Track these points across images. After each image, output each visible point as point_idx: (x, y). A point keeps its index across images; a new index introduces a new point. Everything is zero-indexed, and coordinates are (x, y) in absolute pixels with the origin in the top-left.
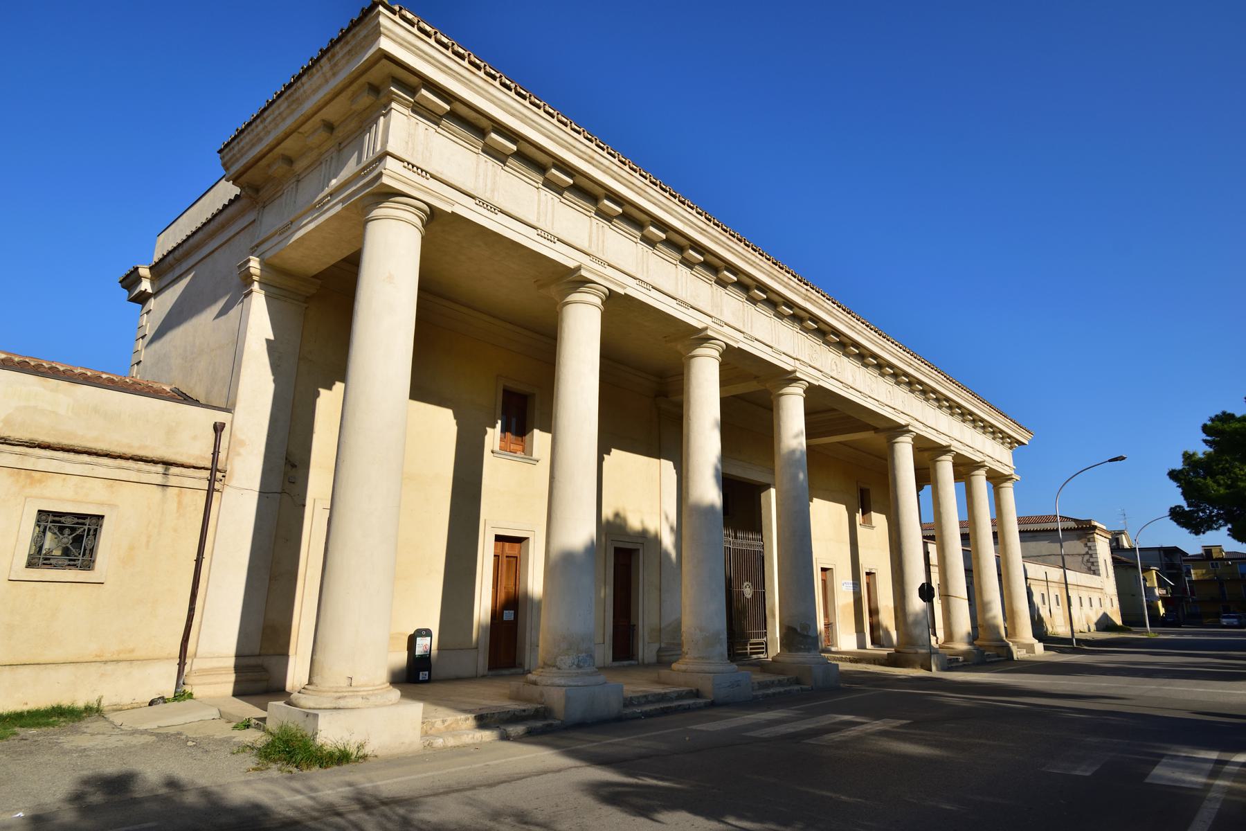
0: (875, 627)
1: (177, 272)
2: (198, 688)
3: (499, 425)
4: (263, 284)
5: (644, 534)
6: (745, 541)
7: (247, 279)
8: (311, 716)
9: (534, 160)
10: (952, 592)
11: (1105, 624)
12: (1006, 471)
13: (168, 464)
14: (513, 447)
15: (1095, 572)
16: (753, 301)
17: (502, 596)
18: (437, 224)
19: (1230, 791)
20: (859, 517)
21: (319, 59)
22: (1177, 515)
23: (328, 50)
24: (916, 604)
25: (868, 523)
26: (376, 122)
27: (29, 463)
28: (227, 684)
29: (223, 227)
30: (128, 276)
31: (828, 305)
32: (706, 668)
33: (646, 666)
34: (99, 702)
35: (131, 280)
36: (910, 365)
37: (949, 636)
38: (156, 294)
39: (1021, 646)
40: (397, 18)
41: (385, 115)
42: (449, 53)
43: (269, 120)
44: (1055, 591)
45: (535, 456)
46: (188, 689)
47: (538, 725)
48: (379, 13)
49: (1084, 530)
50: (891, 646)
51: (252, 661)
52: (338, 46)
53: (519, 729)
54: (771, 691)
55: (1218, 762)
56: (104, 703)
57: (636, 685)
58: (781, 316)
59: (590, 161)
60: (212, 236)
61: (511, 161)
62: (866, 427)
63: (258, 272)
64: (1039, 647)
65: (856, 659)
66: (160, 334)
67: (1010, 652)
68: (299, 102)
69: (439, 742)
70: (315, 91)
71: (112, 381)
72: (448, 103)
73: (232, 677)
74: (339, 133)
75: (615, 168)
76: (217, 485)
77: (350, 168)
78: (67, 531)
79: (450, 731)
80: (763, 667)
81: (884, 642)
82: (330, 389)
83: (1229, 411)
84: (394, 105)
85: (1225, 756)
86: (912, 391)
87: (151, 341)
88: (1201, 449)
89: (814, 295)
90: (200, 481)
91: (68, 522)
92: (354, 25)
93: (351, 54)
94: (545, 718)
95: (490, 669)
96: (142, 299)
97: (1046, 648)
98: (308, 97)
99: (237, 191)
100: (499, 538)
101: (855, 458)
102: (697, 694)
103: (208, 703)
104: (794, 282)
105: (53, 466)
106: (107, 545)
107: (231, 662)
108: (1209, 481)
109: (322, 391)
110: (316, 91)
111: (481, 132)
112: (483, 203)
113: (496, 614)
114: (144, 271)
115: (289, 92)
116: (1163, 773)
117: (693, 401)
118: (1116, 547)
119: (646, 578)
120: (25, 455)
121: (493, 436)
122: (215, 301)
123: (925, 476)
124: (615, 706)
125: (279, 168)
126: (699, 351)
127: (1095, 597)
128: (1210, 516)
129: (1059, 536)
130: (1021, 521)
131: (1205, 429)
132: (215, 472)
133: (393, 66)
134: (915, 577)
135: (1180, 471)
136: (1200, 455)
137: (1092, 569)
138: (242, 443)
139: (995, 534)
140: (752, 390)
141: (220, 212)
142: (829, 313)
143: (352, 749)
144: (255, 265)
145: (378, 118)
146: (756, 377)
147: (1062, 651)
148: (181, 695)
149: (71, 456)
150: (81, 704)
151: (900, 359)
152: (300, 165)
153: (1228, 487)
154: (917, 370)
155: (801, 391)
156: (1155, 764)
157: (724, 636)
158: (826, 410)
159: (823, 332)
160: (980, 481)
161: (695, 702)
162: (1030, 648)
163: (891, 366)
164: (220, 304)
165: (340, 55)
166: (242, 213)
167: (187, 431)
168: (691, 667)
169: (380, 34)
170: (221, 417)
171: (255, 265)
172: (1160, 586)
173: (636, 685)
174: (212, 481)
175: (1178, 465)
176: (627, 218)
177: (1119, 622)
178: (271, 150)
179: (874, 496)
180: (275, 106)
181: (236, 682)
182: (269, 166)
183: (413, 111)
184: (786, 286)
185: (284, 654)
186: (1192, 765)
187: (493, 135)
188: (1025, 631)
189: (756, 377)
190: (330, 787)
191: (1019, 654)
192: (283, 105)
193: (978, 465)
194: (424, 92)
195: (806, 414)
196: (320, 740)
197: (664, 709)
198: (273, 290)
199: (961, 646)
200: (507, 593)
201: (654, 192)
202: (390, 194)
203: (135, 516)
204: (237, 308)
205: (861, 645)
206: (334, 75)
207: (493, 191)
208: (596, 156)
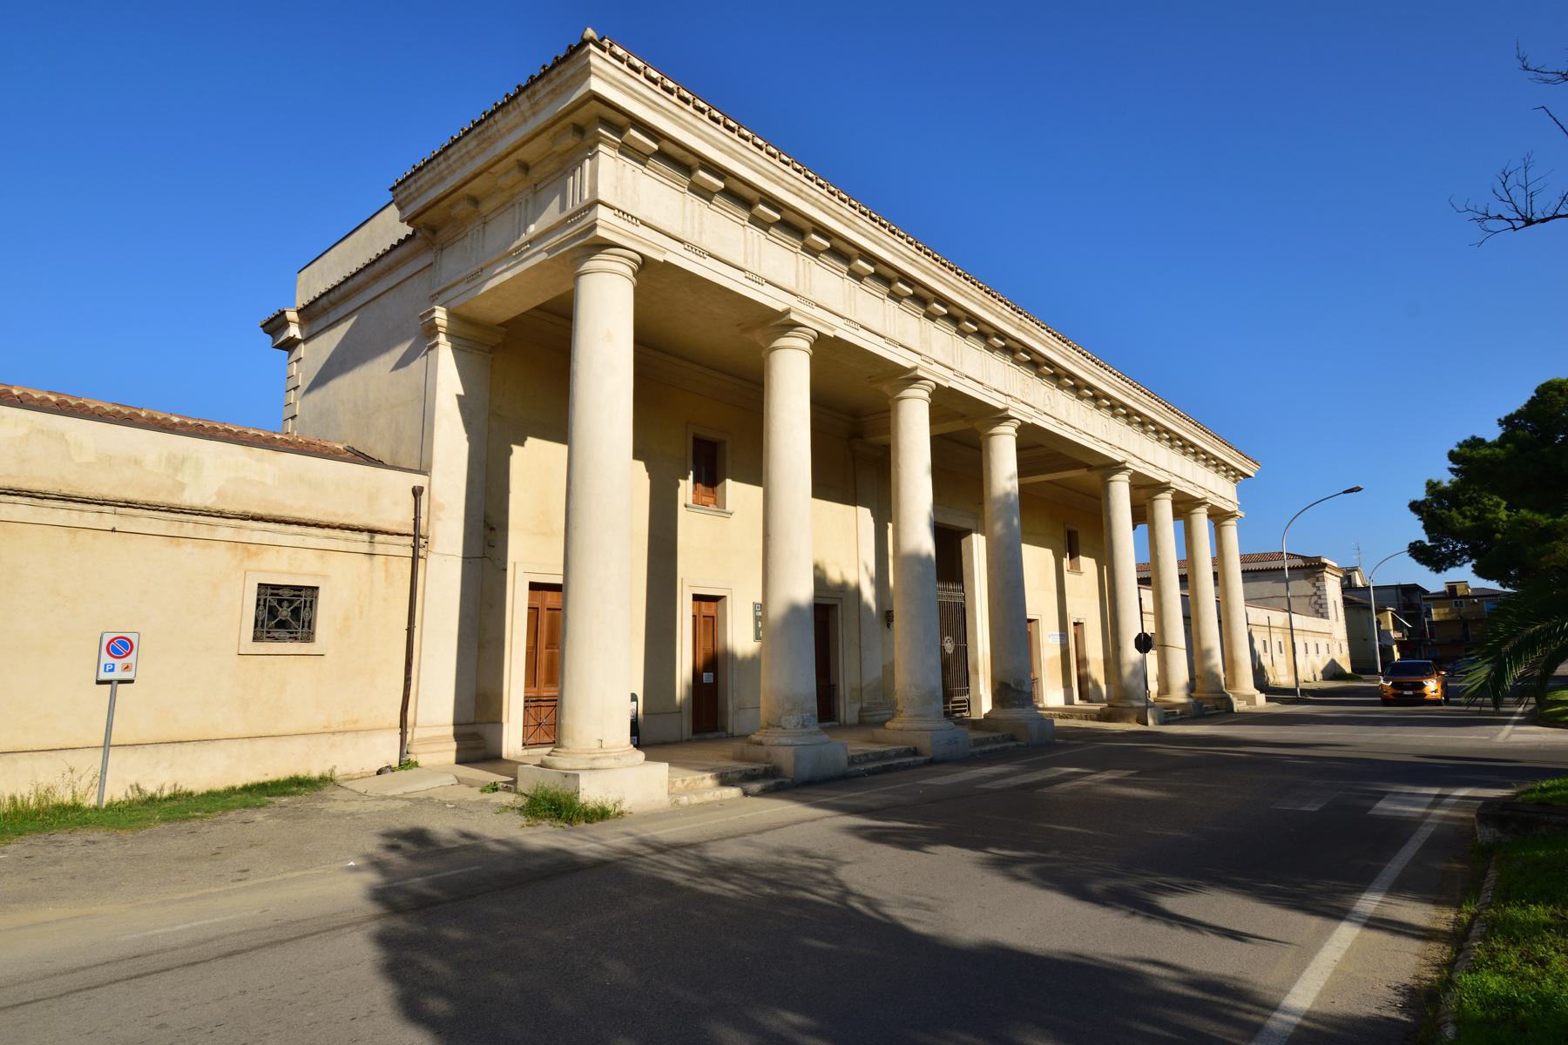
0: (1083, 679)
1: (332, 317)
3: (691, 477)
4: (450, 336)
5: (843, 586)
6: (950, 593)
9: (741, 196)
10: (1169, 641)
11: (1332, 672)
12: (1229, 507)
14: (705, 499)
15: (1324, 615)
16: (963, 333)
17: (700, 662)
18: (650, 275)
19: (1445, 818)
20: (1066, 562)
21: (516, 96)
22: (1417, 551)
23: (527, 87)
24: (1131, 654)
25: (1076, 568)
26: (581, 164)
27: (245, 536)
28: (449, 751)
29: (390, 269)
30: (272, 320)
31: (1043, 334)
34: (332, 771)
35: (275, 325)
36: (1128, 395)
37: (1165, 687)
38: (306, 341)
39: (1242, 698)
40: (607, 56)
41: (591, 158)
42: (641, 77)
43: (453, 158)
44: (1278, 637)
45: (729, 508)
46: (413, 758)
47: (773, 781)
48: (589, 52)
49: (1312, 568)
50: (1101, 701)
51: (469, 729)
52: (540, 84)
53: (755, 787)
54: (987, 748)
55: (1437, 796)
56: (337, 772)
58: (991, 348)
59: (798, 194)
60: (377, 278)
61: (717, 198)
62: (1077, 465)
63: (444, 323)
64: (1261, 699)
65: (1066, 714)
66: (320, 381)
68: (492, 141)
69: (684, 800)
70: (510, 130)
71: (184, 425)
72: (656, 141)
73: (454, 746)
74: (536, 174)
75: (824, 200)
76: (421, 552)
77: (551, 215)
78: (285, 604)
79: (688, 790)
80: (976, 725)
81: (1092, 696)
82: (522, 444)
83: (1479, 436)
84: (601, 147)
85: (1446, 791)
86: (1129, 424)
88: (1446, 478)
89: (1028, 324)
90: (404, 547)
91: (286, 594)
92: (558, 62)
94: (774, 777)
95: (695, 732)
96: (290, 345)
97: (1268, 700)
98: (502, 136)
99: (409, 230)
100: (697, 598)
101: (1068, 499)
103: (436, 771)
104: (1007, 312)
105: (266, 538)
106: (325, 616)
107: (450, 730)
108: (1454, 513)
109: (515, 447)
110: (512, 132)
111: (687, 170)
112: (692, 248)
114: (292, 315)
115: (478, 129)
116: (1385, 807)
117: (901, 446)
118: (1348, 586)
120: (240, 527)
121: (686, 489)
123: (1142, 514)
125: (462, 209)
126: (907, 392)
127: (1323, 642)
128: (1454, 552)
129: (1283, 575)
130: (1244, 559)
132: (418, 538)
133: (603, 107)
134: (1131, 629)
135: (1423, 502)
136: (1446, 484)
137: (1320, 611)
138: (441, 507)
139: (1215, 574)
140: (962, 428)
141: (387, 253)
142: (1043, 342)
143: (610, 808)
144: (441, 315)
145: (583, 161)
146: (963, 416)
147: (1284, 702)
148: (405, 764)
149: (282, 527)
150: (315, 774)
151: (1119, 390)
152: (486, 207)
153: (1474, 519)
154: (1136, 400)
155: (1013, 431)
156: (1379, 799)
157: (940, 693)
158: (1039, 449)
159: (1037, 364)
160: (1201, 519)
161: (909, 761)
162: (1251, 700)
163: (1108, 397)
164: (399, 352)
165: (543, 93)
166: (414, 255)
167: (383, 495)
168: (908, 726)
169: (589, 73)
170: (419, 480)
171: (441, 315)
172: (1395, 629)
174: (415, 548)
175: (1421, 495)
177: (1348, 670)
179: (1082, 538)
180: (461, 143)
181: (458, 750)
182: (451, 206)
183: (621, 152)
184: (999, 316)
185: (498, 722)
187: (701, 173)
188: (1246, 683)
189: (963, 416)
190: (582, 842)
191: (1239, 706)
192: (471, 143)
193: (1198, 503)
194: (633, 132)
195: (1018, 450)
196: (582, 800)
198: (458, 341)
199: (1179, 696)
200: (706, 655)
201: (864, 223)
202: (604, 245)
203: (350, 589)
204: (418, 364)
205: (1069, 700)
206: (534, 114)
207: (701, 233)
208: (805, 188)
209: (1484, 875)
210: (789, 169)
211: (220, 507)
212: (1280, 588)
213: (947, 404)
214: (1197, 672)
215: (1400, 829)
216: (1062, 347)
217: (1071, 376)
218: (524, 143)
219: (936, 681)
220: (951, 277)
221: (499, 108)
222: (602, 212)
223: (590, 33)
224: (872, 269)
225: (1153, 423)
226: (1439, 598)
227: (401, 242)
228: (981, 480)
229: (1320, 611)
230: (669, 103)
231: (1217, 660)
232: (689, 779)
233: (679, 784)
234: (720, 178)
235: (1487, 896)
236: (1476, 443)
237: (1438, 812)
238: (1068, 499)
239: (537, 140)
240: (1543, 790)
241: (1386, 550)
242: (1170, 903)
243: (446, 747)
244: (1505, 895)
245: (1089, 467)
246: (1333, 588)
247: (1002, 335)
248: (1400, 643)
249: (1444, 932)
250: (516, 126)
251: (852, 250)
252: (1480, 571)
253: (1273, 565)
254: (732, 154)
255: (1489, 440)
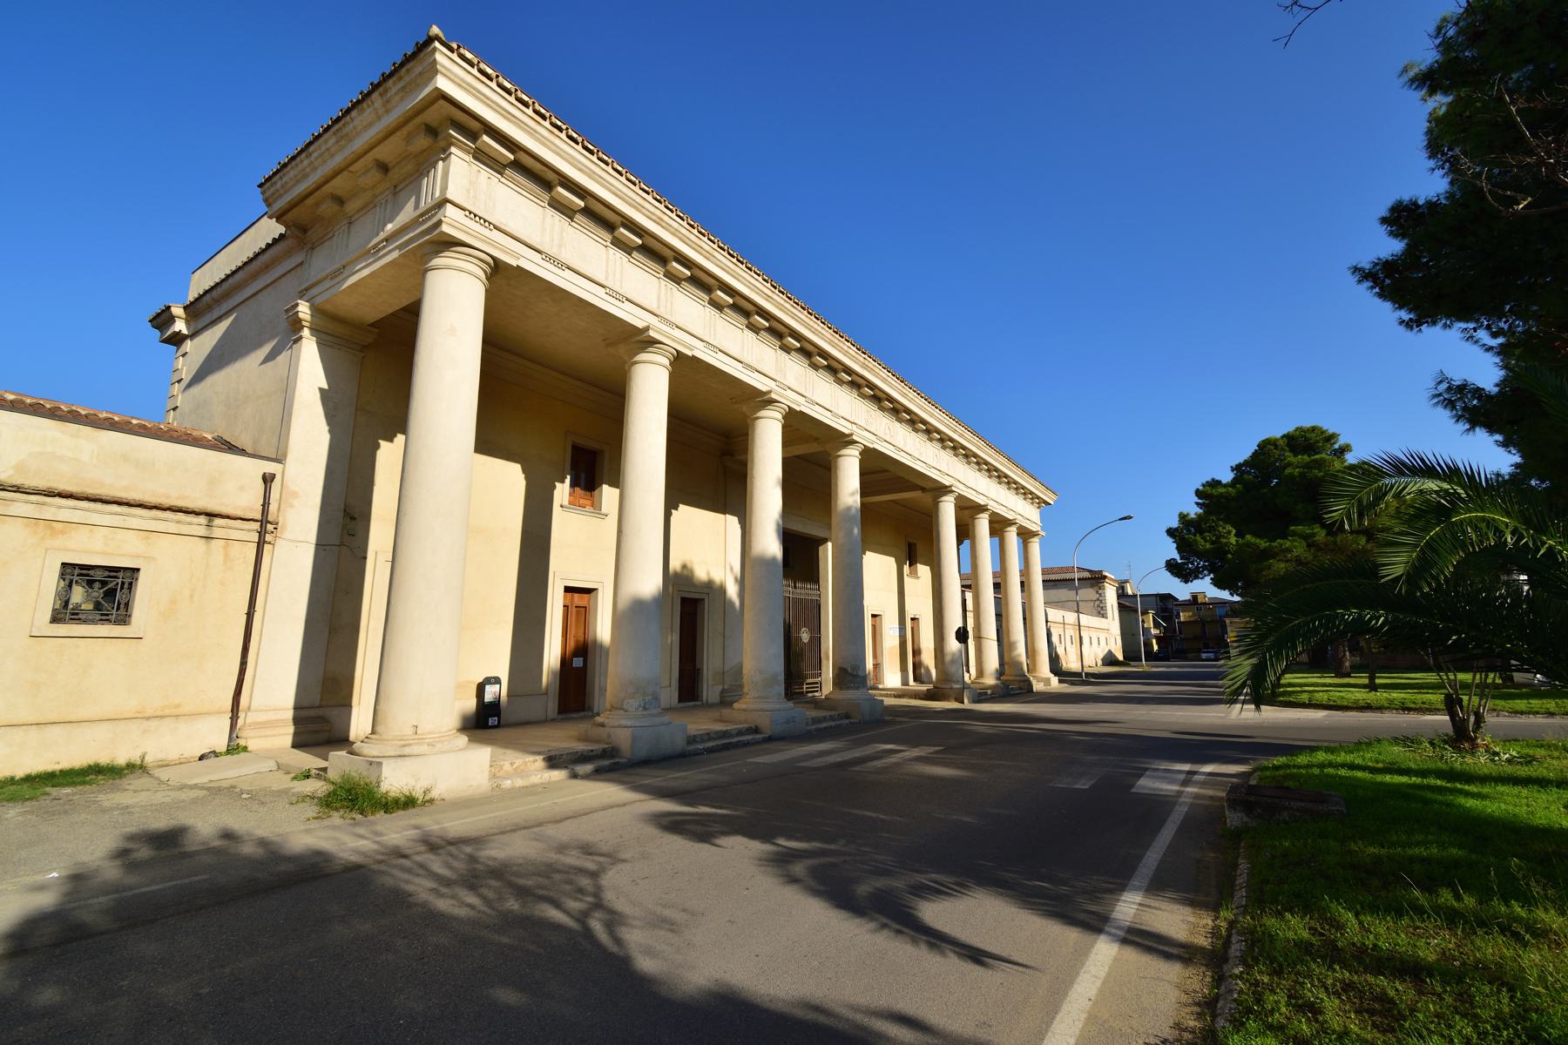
0: (917, 666)
1: (216, 314)
2: (253, 741)
3: (568, 481)
5: (709, 585)
6: (803, 591)
7: (296, 325)
8: (376, 764)
10: (984, 634)
11: (1109, 660)
12: (1034, 528)
13: (211, 515)
15: (1104, 616)
16: (815, 367)
17: (571, 644)
18: (500, 275)
19: (1197, 796)
20: (906, 568)
21: (369, 94)
22: (1172, 567)
25: (914, 574)
26: (434, 165)
27: (49, 513)
29: (267, 268)
30: (158, 315)
32: (765, 706)
33: (710, 706)
35: (162, 320)
37: (980, 673)
38: (192, 336)
39: (1040, 680)
40: (455, 56)
41: (444, 160)
44: (1070, 632)
46: (242, 742)
48: (435, 49)
49: (1096, 579)
53: (588, 768)
55: (1190, 773)
56: (149, 759)
57: (699, 724)
58: (840, 382)
60: (255, 276)
61: (578, 217)
63: (308, 317)
64: (1055, 680)
66: (198, 377)
67: (1031, 685)
68: (349, 138)
69: (508, 784)
73: (291, 729)
74: (395, 175)
76: (268, 538)
77: (407, 214)
78: (97, 585)
79: (519, 772)
80: (817, 704)
84: (453, 149)
87: (190, 385)
88: (1193, 511)
89: (871, 364)
90: (250, 533)
91: (99, 575)
92: (408, 59)
93: (407, 91)
94: (612, 757)
96: (177, 340)
98: (358, 134)
99: (282, 229)
101: (904, 515)
102: (756, 730)
103: (266, 755)
105: (77, 516)
107: (290, 714)
108: (1198, 538)
110: (368, 128)
112: (549, 258)
113: (565, 661)
114: (177, 311)
116: (1146, 784)
118: (1122, 594)
119: (711, 625)
120: (43, 504)
121: (562, 491)
122: (260, 345)
123: (965, 532)
124: (680, 743)
125: (328, 208)
126: (763, 413)
127: (1103, 637)
129: (1074, 584)
130: (1044, 572)
131: (1198, 493)
132: (265, 525)
133: (453, 109)
134: (954, 621)
137: (1101, 613)
138: (295, 494)
139: (1022, 583)
140: (812, 452)
142: (884, 380)
143: (418, 794)
144: (304, 310)
146: (816, 439)
147: (1073, 683)
149: (99, 506)
150: (121, 761)
152: (351, 207)
154: (961, 436)
156: (1140, 776)
158: (878, 470)
159: (879, 398)
162: (1047, 681)
164: (267, 349)
166: (288, 254)
167: (234, 482)
169: (436, 72)
170: (270, 467)
171: (304, 310)
173: (699, 724)
174: (262, 533)
175: (1175, 524)
176: (695, 281)
177: (1121, 658)
178: (318, 188)
179: (920, 549)
180: (321, 140)
181: (296, 734)
182: (317, 205)
184: (846, 354)
185: (347, 705)
186: (1167, 775)
187: (560, 189)
189: (816, 439)
191: (1038, 687)
193: (1010, 523)
194: (485, 138)
196: (384, 787)
197: (725, 744)
200: (577, 642)
201: (722, 257)
204: (283, 358)
205: (905, 682)
206: (387, 111)
207: (560, 246)
208: (665, 218)
209: (1235, 866)
210: (649, 198)
211: (18, 481)
212: (1071, 594)
213: (799, 427)
214: (1006, 659)
215: (1159, 806)
216: (900, 386)
217: (908, 411)
218: (379, 142)
219: (779, 666)
220: (803, 315)
221: (355, 105)
222: (450, 210)
223: (435, 30)
224: (731, 301)
225: (975, 456)
226: (1186, 605)
227: (275, 241)
228: (829, 495)
229: (1101, 613)
230: (526, 116)
231: (1021, 650)
232: (518, 762)
233: (507, 767)
234: (581, 197)
235: (1241, 895)
236: (1215, 483)
237: (1189, 789)
238: (904, 515)
239: (392, 139)
240: (1276, 768)
241: (1148, 566)
242: (934, 912)
243: (282, 731)
244: (1260, 900)
245: (923, 489)
246: (1111, 594)
247: (849, 371)
248: (1157, 637)
249: (1203, 949)
250: (370, 125)
251: (712, 281)
252: (1218, 583)
253: (1068, 576)
254: (591, 175)
255: (1224, 481)
